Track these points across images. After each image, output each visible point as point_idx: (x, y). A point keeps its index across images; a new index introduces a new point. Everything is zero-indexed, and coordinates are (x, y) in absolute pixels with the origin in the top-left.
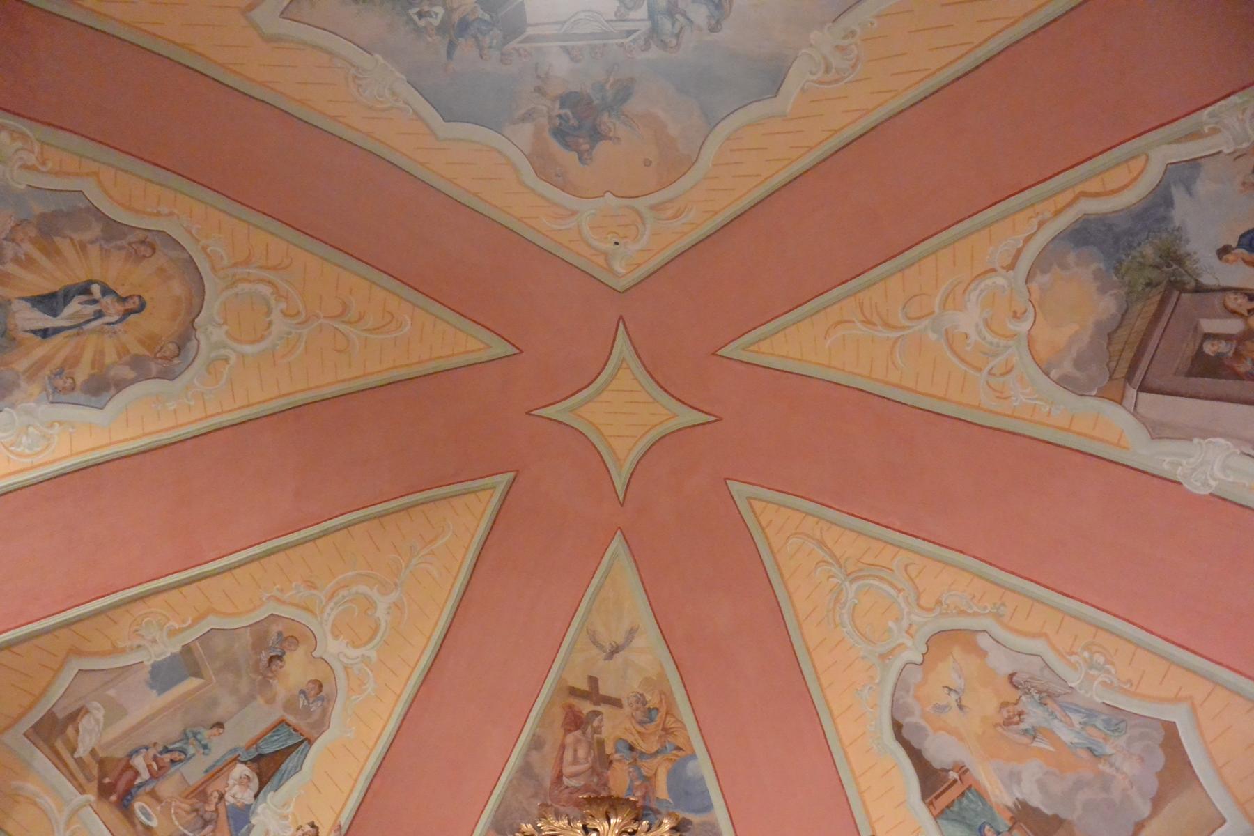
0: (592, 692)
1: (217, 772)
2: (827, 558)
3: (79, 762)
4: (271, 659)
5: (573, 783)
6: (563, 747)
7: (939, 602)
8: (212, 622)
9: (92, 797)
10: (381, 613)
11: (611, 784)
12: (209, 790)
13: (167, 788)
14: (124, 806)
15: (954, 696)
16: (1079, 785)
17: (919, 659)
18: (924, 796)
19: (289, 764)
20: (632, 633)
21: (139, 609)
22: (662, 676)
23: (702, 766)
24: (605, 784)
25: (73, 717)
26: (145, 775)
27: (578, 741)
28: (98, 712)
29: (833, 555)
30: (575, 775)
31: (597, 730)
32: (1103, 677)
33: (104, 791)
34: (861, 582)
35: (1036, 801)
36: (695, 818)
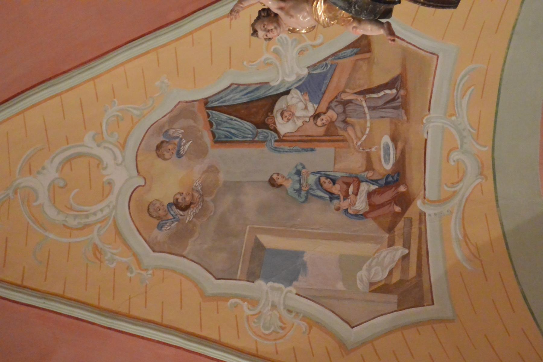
1: (304, 142)
3: (407, 245)
9: (419, 204)
10: (51, 173)
12: (321, 131)
13: (354, 163)
19: (238, 98)
25: (383, 288)
26: (365, 188)
33: (405, 201)
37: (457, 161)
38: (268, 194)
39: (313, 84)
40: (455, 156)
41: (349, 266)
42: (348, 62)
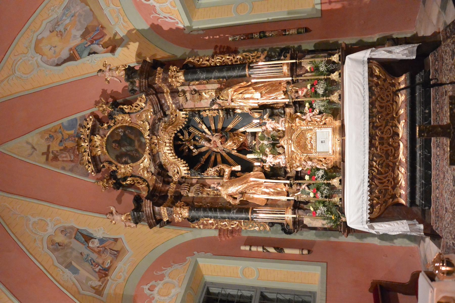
0: (46, 154)
1: (92, 250)
2: (7, 80)
3: (102, 283)
4: (60, 246)
5: (72, 157)
6: (63, 161)
7: (27, 48)
8: (56, 263)
9: (109, 277)
10: (36, 219)
11: (71, 146)
12: (97, 251)
13: (100, 261)
14: (107, 270)
15: (52, 48)
16: (80, 21)
17: (41, 56)
18: (76, 60)
19: (85, 233)
20: (28, 143)
21: (62, 282)
22: (40, 133)
23: (65, 121)
24: (72, 148)
25: (94, 288)
26: (99, 267)
27: (61, 157)
28: (90, 283)
29: (7, 77)
30: (71, 157)
31: (57, 152)
32: (57, 9)
33: (106, 275)
34: (16, 70)
35: (81, 32)
36: (79, 123)
37: (121, 275)
38: (80, 255)
39: (102, 241)
40: (121, 273)
41: (88, 279)
42: (111, 241)
